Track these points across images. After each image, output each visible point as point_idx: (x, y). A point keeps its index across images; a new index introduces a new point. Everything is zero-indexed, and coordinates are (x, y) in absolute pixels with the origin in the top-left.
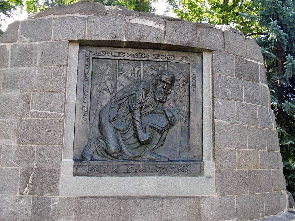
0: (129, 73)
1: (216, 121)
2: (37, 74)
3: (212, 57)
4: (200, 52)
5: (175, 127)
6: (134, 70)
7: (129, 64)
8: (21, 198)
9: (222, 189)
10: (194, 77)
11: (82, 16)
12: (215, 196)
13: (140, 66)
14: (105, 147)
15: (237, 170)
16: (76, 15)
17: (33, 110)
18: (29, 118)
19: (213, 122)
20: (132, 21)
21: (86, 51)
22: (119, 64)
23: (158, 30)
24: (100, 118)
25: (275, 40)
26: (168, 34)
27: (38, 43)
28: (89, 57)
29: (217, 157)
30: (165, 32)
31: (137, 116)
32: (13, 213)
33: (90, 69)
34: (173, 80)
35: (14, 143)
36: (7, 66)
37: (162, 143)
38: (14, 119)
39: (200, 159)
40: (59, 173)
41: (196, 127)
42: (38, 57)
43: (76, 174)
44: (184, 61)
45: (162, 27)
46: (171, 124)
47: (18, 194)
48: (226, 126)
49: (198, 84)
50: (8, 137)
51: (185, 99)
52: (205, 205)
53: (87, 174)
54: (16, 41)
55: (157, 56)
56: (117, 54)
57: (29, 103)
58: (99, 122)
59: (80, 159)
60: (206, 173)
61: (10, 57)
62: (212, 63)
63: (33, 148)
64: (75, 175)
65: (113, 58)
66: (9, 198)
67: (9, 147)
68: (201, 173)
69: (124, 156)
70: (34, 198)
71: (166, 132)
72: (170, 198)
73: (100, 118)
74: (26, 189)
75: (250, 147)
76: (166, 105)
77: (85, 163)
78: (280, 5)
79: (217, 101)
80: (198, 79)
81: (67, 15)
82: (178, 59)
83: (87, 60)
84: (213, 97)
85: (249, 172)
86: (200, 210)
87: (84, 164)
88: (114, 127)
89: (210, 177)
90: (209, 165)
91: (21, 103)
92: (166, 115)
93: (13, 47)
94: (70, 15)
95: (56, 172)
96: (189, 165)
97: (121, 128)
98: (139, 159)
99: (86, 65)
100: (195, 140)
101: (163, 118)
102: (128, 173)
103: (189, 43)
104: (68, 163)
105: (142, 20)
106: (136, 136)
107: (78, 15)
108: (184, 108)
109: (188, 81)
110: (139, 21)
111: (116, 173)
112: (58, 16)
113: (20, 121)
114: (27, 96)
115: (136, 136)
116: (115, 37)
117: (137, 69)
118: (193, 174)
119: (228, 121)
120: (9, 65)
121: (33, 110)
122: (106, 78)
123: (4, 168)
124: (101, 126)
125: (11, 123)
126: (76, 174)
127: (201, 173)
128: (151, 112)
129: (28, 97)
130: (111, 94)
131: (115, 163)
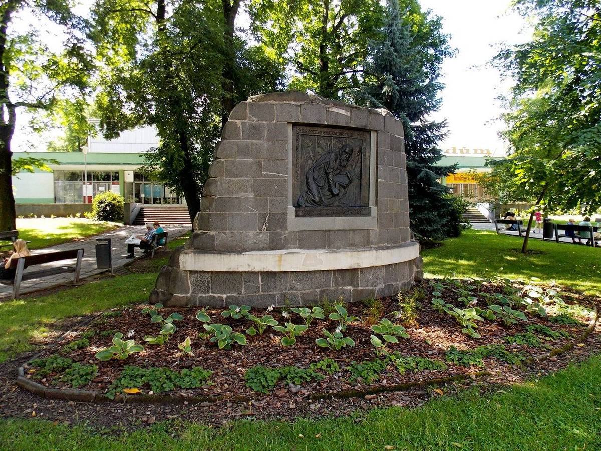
0: (325, 146)
1: (379, 180)
2: (266, 146)
3: (377, 136)
4: (369, 132)
5: (352, 184)
6: (327, 144)
9: (380, 225)
10: (365, 149)
11: (295, 103)
12: (377, 229)
13: (330, 140)
14: (312, 198)
16: (291, 102)
17: (265, 173)
19: (377, 181)
20: (330, 110)
21: (298, 129)
22: (318, 140)
23: (347, 116)
24: (307, 179)
25: (388, 93)
26: (353, 119)
27: (265, 123)
29: (379, 204)
31: (330, 177)
32: (255, 242)
33: (300, 143)
34: (352, 151)
35: (252, 196)
36: (240, 139)
38: (250, 179)
39: (367, 205)
40: (287, 216)
41: (365, 184)
42: (266, 134)
43: (297, 216)
44: (359, 138)
45: (349, 114)
46: (350, 182)
47: (258, 230)
48: (384, 184)
49: (367, 154)
50: (246, 192)
51: (359, 165)
52: (372, 234)
53: (303, 216)
54: (246, 119)
55: (341, 134)
56: (317, 132)
57: (261, 167)
58: (305, 180)
59: (297, 206)
60: (372, 215)
61: (241, 132)
62: (377, 139)
63: (267, 199)
64: (296, 217)
66: (251, 233)
67: (248, 199)
68: (369, 214)
70: (270, 233)
72: (354, 230)
73: (307, 179)
74: (264, 226)
75: (395, 197)
76: (347, 169)
77: (301, 209)
78: (395, 57)
79: (379, 166)
80: (367, 150)
81: (285, 102)
83: (298, 136)
84: (377, 164)
86: (369, 238)
87: (301, 210)
88: (307, 183)
89: (374, 217)
90: (374, 210)
91: (255, 167)
92: (348, 176)
93: (243, 124)
94: (288, 102)
95: (285, 215)
96: (361, 210)
97: (321, 185)
98: (331, 206)
99: (297, 140)
100: (364, 193)
101: (346, 178)
102: (327, 215)
103: (365, 126)
104: (291, 209)
106: (330, 190)
107: (293, 102)
108: (357, 171)
109: (360, 151)
110: (335, 110)
111: (320, 215)
112: (278, 102)
113: (255, 180)
114: (259, 162)
115: (330, 190)
116: (319, 121)
117: (329, 143)
118: (364, 215)
120: (241, 138)
121: (265, 173)
122: (310, 149)
123: (245, 213)
124: (307, 183)
125: (248, 182)
126: (297, 216)
127: (369, 214)
128: (338, 174)
129: (260, 163)
130: (313, 161)
131: (319, 208)
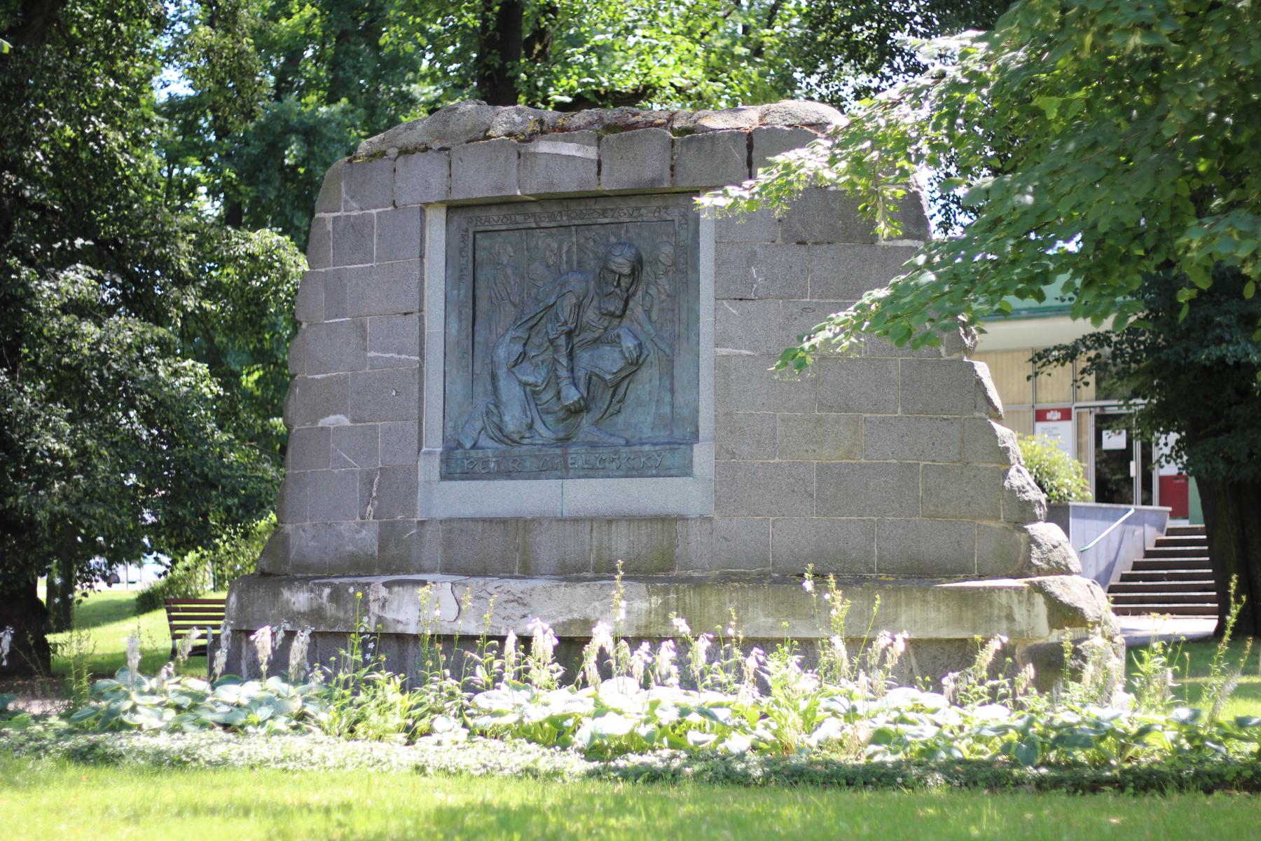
7: (551, 235)
8: (363, 524)
15: (777, 460)
18: (367, 370)
28: (467, 231)
30: (599, 163)
37: (617, 407)
47: (358, 519)
60: (697, 470)
63: (375, 428)
65: (515, 227)
69: (537, 437)
70: (381, 525)
71: (626, 383)
74: (369, 508)
82: (646, 214)
85: (821, 468)
90: (703, 455)
103: (653, 181)
105: (549, 143)
116: (500, 189)
119: (755, 349)
123: (336, 471)
129: (363, 327)
